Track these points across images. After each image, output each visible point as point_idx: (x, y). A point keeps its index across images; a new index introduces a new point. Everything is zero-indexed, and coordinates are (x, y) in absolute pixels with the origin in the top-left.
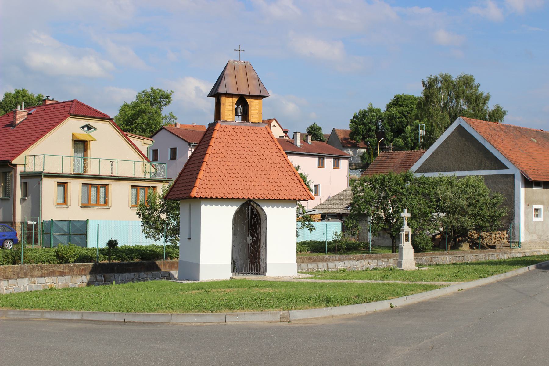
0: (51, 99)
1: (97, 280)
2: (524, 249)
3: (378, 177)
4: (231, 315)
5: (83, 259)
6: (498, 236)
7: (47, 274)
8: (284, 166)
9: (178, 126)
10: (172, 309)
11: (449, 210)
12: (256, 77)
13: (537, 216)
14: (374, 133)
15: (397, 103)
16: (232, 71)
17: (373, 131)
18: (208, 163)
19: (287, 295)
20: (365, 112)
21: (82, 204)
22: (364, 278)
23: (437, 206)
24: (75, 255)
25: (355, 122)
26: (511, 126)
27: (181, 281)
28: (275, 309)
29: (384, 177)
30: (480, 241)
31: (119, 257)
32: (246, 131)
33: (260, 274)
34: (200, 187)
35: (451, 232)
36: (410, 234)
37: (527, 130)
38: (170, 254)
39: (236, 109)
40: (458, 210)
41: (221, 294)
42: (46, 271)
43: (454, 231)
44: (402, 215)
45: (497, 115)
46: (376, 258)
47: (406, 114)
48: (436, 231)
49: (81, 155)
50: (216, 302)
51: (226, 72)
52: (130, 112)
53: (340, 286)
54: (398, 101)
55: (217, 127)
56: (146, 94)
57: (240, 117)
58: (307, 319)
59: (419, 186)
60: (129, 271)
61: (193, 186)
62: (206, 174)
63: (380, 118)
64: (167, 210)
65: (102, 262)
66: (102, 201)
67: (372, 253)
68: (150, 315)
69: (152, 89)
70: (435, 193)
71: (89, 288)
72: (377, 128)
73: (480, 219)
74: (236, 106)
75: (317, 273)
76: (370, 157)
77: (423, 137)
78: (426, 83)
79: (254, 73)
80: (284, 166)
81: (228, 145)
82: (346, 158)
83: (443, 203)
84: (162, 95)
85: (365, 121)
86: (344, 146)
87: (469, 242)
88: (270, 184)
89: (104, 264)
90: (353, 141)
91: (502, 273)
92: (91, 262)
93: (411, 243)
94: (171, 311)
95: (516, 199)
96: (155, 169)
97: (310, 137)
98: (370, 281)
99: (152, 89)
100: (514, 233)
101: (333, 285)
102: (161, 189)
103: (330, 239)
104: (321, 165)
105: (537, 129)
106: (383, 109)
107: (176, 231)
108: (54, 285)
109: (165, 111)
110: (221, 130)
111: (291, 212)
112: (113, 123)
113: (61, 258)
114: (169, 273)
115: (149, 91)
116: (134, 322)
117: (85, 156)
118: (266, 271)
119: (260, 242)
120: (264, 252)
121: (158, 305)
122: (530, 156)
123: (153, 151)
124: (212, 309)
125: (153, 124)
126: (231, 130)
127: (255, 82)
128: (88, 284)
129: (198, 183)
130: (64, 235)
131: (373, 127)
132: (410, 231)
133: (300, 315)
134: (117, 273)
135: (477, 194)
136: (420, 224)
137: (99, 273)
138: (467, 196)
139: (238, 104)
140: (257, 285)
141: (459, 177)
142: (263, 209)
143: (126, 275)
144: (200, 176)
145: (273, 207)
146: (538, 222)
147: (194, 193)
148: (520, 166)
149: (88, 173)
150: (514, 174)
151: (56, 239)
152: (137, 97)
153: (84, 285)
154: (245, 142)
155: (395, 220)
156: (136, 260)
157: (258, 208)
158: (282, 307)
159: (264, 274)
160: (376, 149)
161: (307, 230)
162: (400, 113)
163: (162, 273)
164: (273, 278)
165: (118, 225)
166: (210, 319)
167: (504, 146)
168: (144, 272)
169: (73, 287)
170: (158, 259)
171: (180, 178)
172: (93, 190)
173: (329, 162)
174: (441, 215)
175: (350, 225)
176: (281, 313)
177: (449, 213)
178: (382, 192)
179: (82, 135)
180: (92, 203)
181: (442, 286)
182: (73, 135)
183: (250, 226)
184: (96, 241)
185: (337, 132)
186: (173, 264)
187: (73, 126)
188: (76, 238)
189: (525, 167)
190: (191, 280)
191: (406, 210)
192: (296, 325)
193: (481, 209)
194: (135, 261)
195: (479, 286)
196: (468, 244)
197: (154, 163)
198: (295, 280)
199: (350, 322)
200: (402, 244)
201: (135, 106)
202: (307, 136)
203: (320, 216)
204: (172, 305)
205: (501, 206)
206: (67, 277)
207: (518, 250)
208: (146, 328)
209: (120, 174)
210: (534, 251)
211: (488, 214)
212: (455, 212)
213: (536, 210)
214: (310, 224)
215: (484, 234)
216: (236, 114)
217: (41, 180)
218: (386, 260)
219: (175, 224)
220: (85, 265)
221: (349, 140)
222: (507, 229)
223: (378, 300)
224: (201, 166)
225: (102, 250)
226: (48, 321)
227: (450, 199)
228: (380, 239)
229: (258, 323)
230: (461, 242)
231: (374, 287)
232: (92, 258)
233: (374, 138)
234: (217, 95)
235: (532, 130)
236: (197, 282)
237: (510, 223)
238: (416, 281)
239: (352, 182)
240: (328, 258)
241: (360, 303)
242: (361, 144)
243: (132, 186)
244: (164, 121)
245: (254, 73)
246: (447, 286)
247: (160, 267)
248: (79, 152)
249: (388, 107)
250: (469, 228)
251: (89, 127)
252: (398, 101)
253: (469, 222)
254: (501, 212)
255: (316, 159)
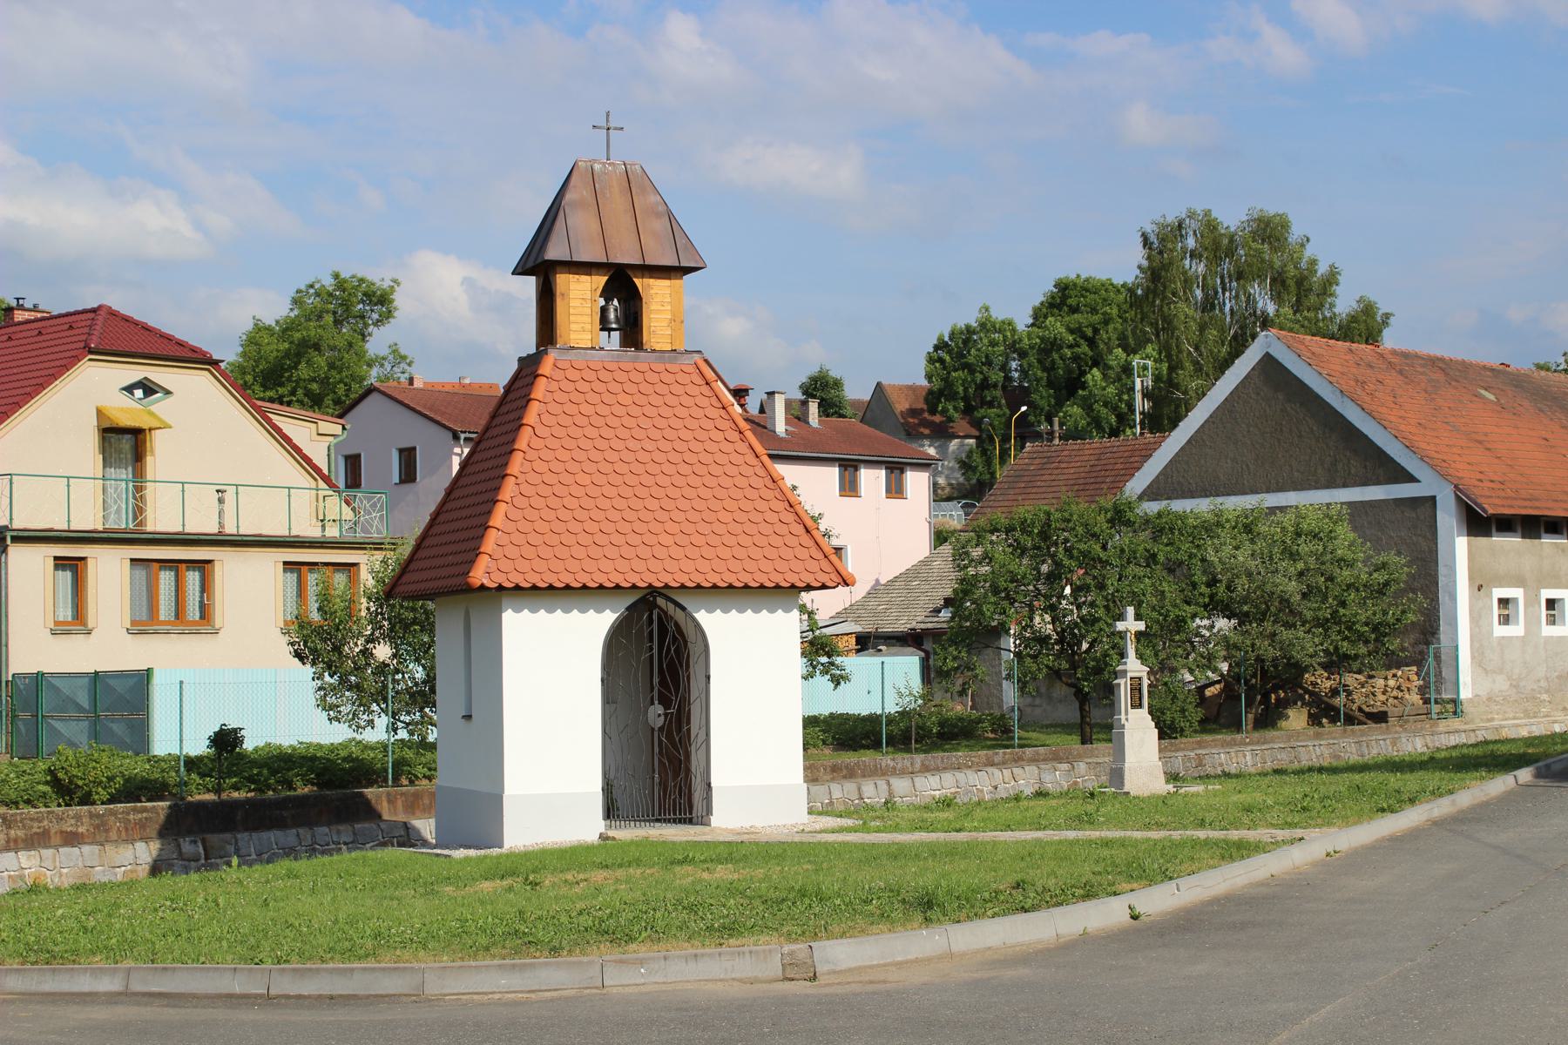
0: (28, 305)
1: (181, 856)
2: (1472, 721)
3: (1029, 517)
4: (621, 962)
5: (134, 790)
6: (1392, 683)
7: (24, 841)
8: (756, 482)
9: (418, 384)
10: (425, 947)
11: (1246, 608)
12: (661, 208)
13: (1505, 620)
14: (998, 393)
15: (1063, 303)
16: (587, 193)
17: (995, 386)
18: (522, 478)
19: (787, 892)
20: (969, 330)
21: (133, 623)
22: (1020, 825)
23: (1212, 597)
24: (110, 779)
25: (941, 361)
26: (1417, 356)
27: (446, 852)
28: (763, 938)
29: (1048, 514)
30: (1340, 701)
31: (251, 780)
32: (637, 377)
33: (690, 822)
34: (498, 553)
35: (1254, 675)
36: (1146, 682)
37: (1465, 367)
38: (407, 765)
39: (604, 310)
40: (1273, 609)
41: (577, 890)
42: (20, 833)
43: (1264, 672)
44: (1120, 626)
45: (1364, 327)
46: (1034, 760)
47: (1089, 332)
48: (1210, 674)
49: (125, 473)
50: (564, 919)
51: (569, 196)
52: (274, 348)
53: (952, 851)
54: (1064, 298)
55: (546, 368)
56: (317, 294)
57: (616, 335)
58: (871, 967)
59: (1154, 539)
60: (280, 824)
61: (475, 553)
62: (514, 514)
63: (1015, 347)
64: (398, 631)
65: (198, 797)
66: (193, 612)
67: (1021, 746)
68: (352, 970)
69: (336, 276)
70: (1203, 560)
71: (155, 881)
72: (1008, 379)
73: (1339, 632)
74: (602, 302)
75: (860, 812)
76: (989, 463)
77: (1146, 394)
78: (1153, 238)
79: (654, 198)
80: (756, 482)
81: (580, 420)
82: (924, 465)
83: (1228, 588)
84: (365, 294)
85: (971, 359)
86: (911, 434)
87: (1309, 704)
88: (714, 540)
89: (202, 805)
90: (938, 419)
91: (1441, 795)
92: (161, 799)
93: (1150, 713)
94: (422, 953)
95: (1442, 570)
96: (353, 510)
97: (813, 407)
98: (1039, 834)
99: (336, 276)
100: (1439, 674)
101: (933, 851)
102: (370, 569)
103: (892, 708)
104: (849, 488)
105: (1494, 361)
106: (1023, 321)
107: (423, 696)
108: (50, 879)
109: (378, 342)
110: (558, 375)
111: (779, 630)
112: (223, 373)
113: (67, 790)
114: (406, 826)
115: (328, 282)
116: (299, 997)
117: (139, 473)
118: (709, 811)
119: (689, 722)
120: (702, 751)
121: (377, 935)
122: (1480, 442)
123: (347, 458)
124: (555, 943)
125: (341, 381)
126: (590, 376)
127: (661, 225)
128: (156, 869)
129: (490, 542)
130: (78, 719)
131: (996, 376)
132: (1144, 675)
133: (846, 956)
134: (246, 830)
135: (1329, 557)
136: (1162, 655)
137: (189, 832)
138: (1300, 566)
139: (607, 293)
140: (683, 857)
141: (1273, 510)
142: (694, 619)
143: (273, 836)
144: (498, 519)
145: (741, 611)
146: (1511, 638)
147: (480, 574)
148: (1451, 471)
149: (149, 528)
150: (1433, 498)
151: (55, 733)
152: (295, 301)
153: (143, 870)
154: (635, 411)
155: (1085, 646)
156: (303, 790)
157: (679, 616)
158: (785, 930)
159: (704, 820)
160: (1005, 439)
161: (822, 682)
162: (1072, 331)
163: (383, 826)
164: (732, 831)
165: (242, 684)
166: (552, 978)
167: (1402, 413)
168: (329, 824)
169: (105, 879)
170: (370, 784)
171: (435, 530)
172: (166, 578)
173: (872, 479)
174: (1222, 624)
175: (950, 664)
176: (786, 949)
177: (1243, 618)
178: (1044, 562)
179: (128, 411)
180: (162, 618)
181: (1276, 844)
182: (100, 413)
183: (656, 671)
184: (179, 732)
185: (889, 392)
186: (417, 796)
187: (97, 386)
188: (114, 727)
189: (1468, 477)
190: (478, 848)
191: (1131, 611)
192: (839, 990)
193: (1343, 604)
194: (299, 792)
195: (1383, 839)
196: (1305, 711)
197: (352, 492)
198: (806, 838)
199: (1009, 974)
200: (1123, 717)
201: (288, 328)
202: (804, 403)
203: (853, 641)
204: (423, 934)
205: (1401, 593)
206: (86, 849)
207: (1455, 723)
208: (342, 1015)
209: (248, 528)
210: (1502, 727)
211: (1363, 618)
212: (1264, 614)
213: (1504, 602)
214: (832, 664)
215: (1350, 679)
216: (605, 326)
217: (5, 550)
218: (1065, 766)
219: (420, 674)
220: (145, 810)
221: (926, 415)
222: (1419, 661)
223: (1089, 894)
224: (498, 489)
225: (192, 763)
226: (12, 1002)
227: (1249, 575)
228: (1038, 701)
229: (710, 986)
230: (1284, 704)
231: (1063, 853)
232: (164, 786)
233: (1000, 406)
234: (540, 266)
235: (1477, 365)
236: (495, 851)
237: (1428, 643)
238: (1185, 828)
239: (940, 537)
240: (892, 764)
241: (1034, 908)
242: (961, 425)
243: (285, 563)
244: (374, 372)
245: (654, 198)
246: (1292, 842)
247: (379, 808)
248: (119, 464)
249: (1039, 316)
250: (1307, 661)
251: (149, 388)
252: (1064, 298)
253: (1306, 644)
254: (1403, 612)
255: (835, 471)
